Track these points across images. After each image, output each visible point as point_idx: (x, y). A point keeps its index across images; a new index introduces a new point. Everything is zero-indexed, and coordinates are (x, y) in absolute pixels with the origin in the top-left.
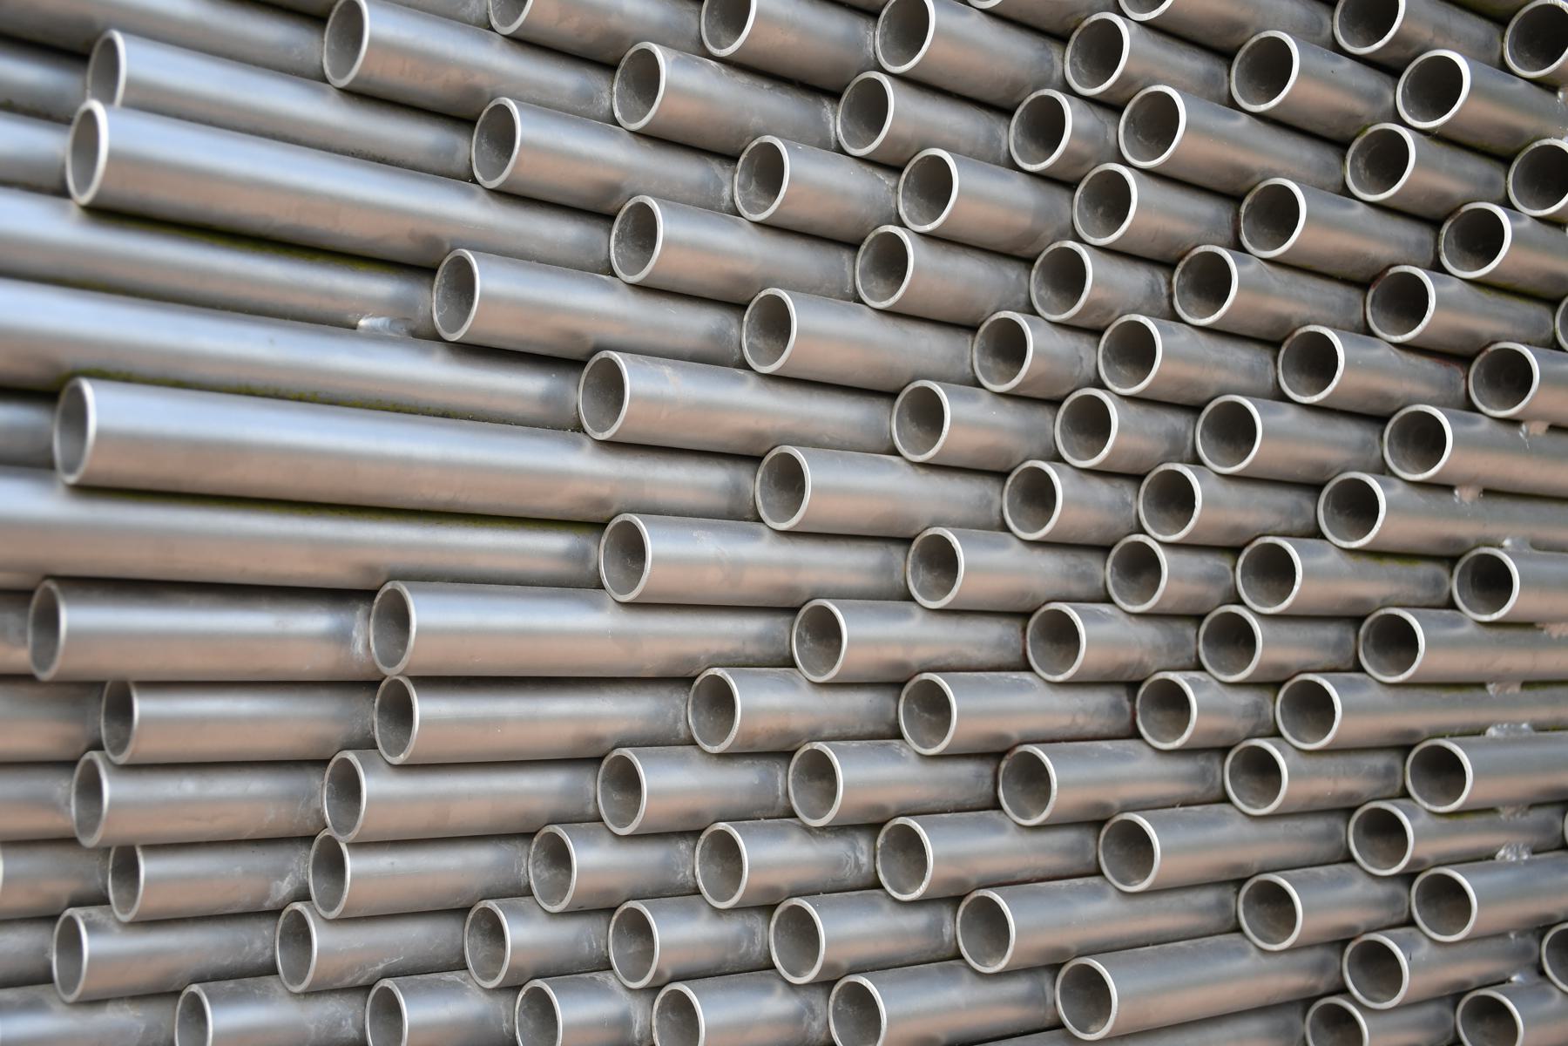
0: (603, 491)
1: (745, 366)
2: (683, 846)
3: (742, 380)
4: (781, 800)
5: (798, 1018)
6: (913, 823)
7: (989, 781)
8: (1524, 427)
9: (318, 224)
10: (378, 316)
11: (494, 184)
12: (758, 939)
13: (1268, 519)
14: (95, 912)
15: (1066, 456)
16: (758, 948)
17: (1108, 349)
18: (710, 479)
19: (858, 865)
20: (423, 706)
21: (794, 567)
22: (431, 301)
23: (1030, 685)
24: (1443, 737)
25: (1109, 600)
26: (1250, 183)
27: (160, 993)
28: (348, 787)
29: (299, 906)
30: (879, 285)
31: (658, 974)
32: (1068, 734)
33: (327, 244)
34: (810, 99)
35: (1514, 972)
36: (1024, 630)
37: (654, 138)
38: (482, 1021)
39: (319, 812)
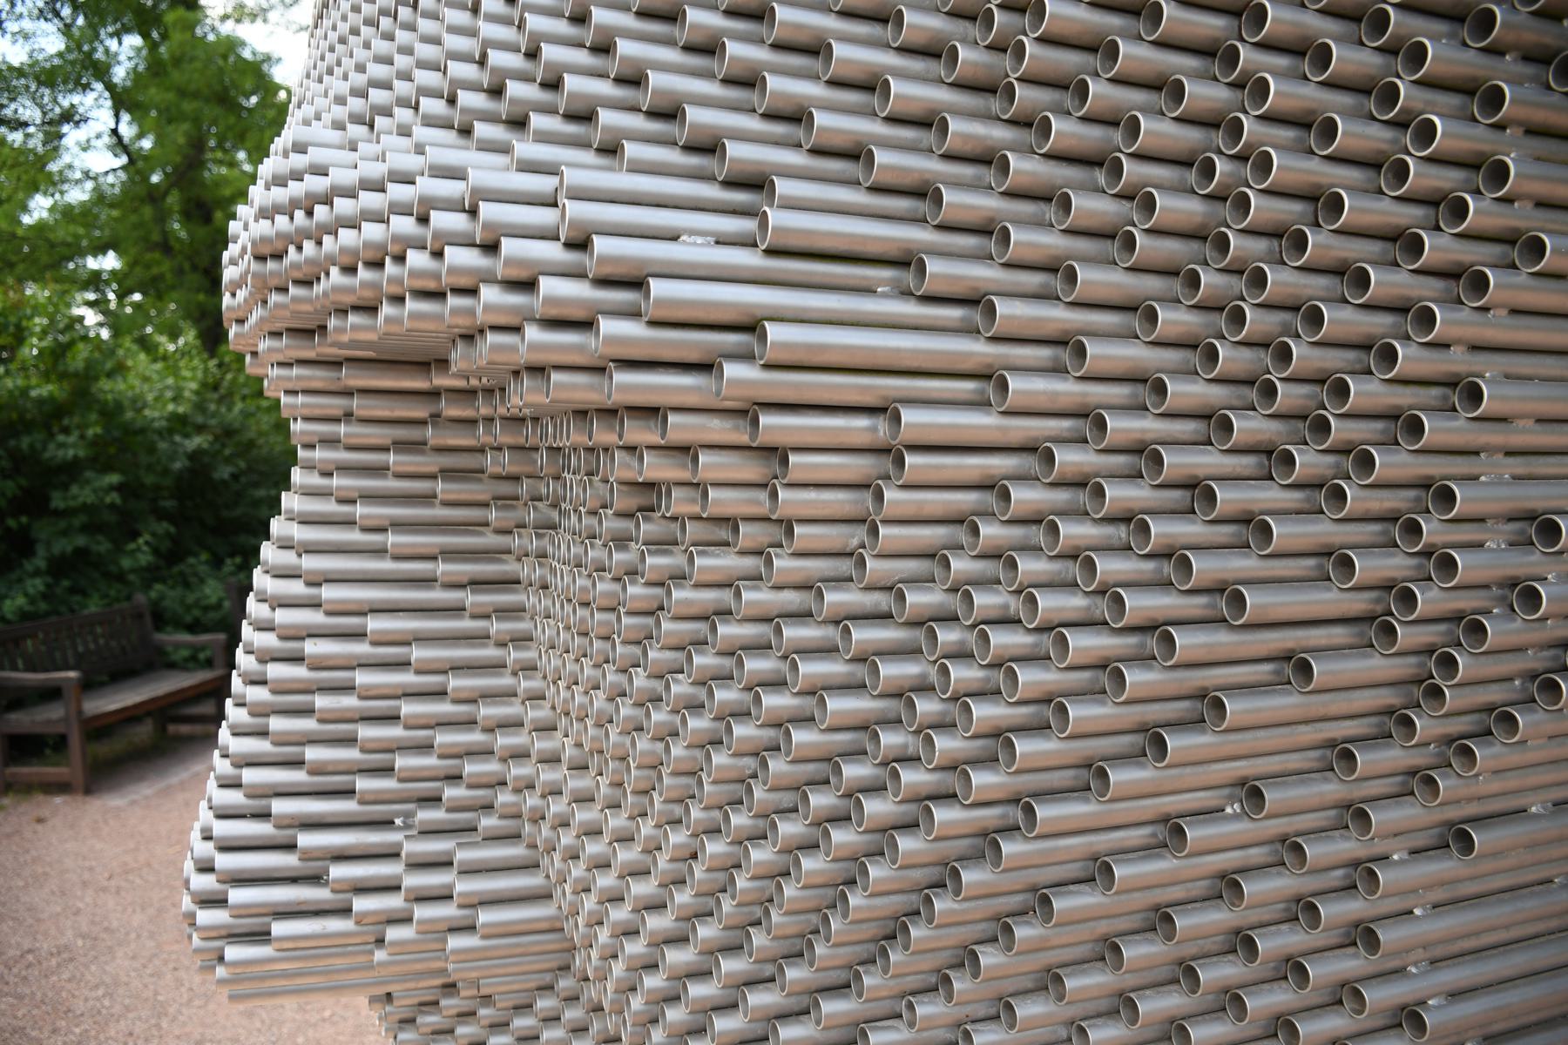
0: (990, 360)
1: (1058, 298)
2: (1034, 528)
3: (1057, 305)
4: (1082, 507)
5: (1088, 608)
6: (1146, 517)
7: (1189, 499)
8: (1492, 312)
9: (857, 248)
10: (885, 286)
11: (935, 223)
12: (1071, 571)
13: (1339, 365)
14: (778, 550)
15: (1227, 336)
16: (1070, 576)
17: (1247, 280)
18: (1043, 354)
19: (1120, 539)
20: (910, 459)
21: (1085, 395)
22: (909, 278)
23: (1209, 451)
24: (1450, 480)
25: (1254, 409)
26: (1322, 191)
27: (805, 587)
28: (879, 496)
29: (861, 550)
30: (1125, 255)
31: (1020, 583)
32: (1232, 476)
33: (863, 256)
34: (1088, 168)
35: (1495, 607)
36: (1209, 425)
37: (1010, 194)
38: (941, 605)
39: (868, 508)
